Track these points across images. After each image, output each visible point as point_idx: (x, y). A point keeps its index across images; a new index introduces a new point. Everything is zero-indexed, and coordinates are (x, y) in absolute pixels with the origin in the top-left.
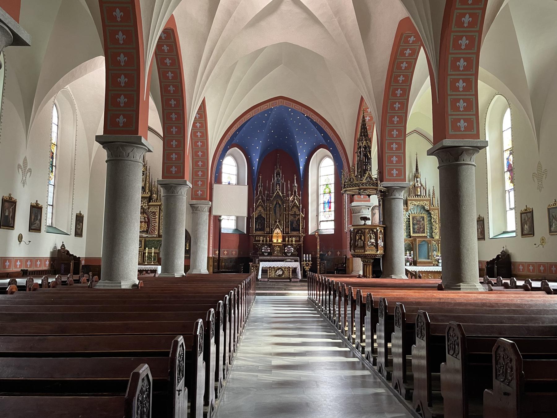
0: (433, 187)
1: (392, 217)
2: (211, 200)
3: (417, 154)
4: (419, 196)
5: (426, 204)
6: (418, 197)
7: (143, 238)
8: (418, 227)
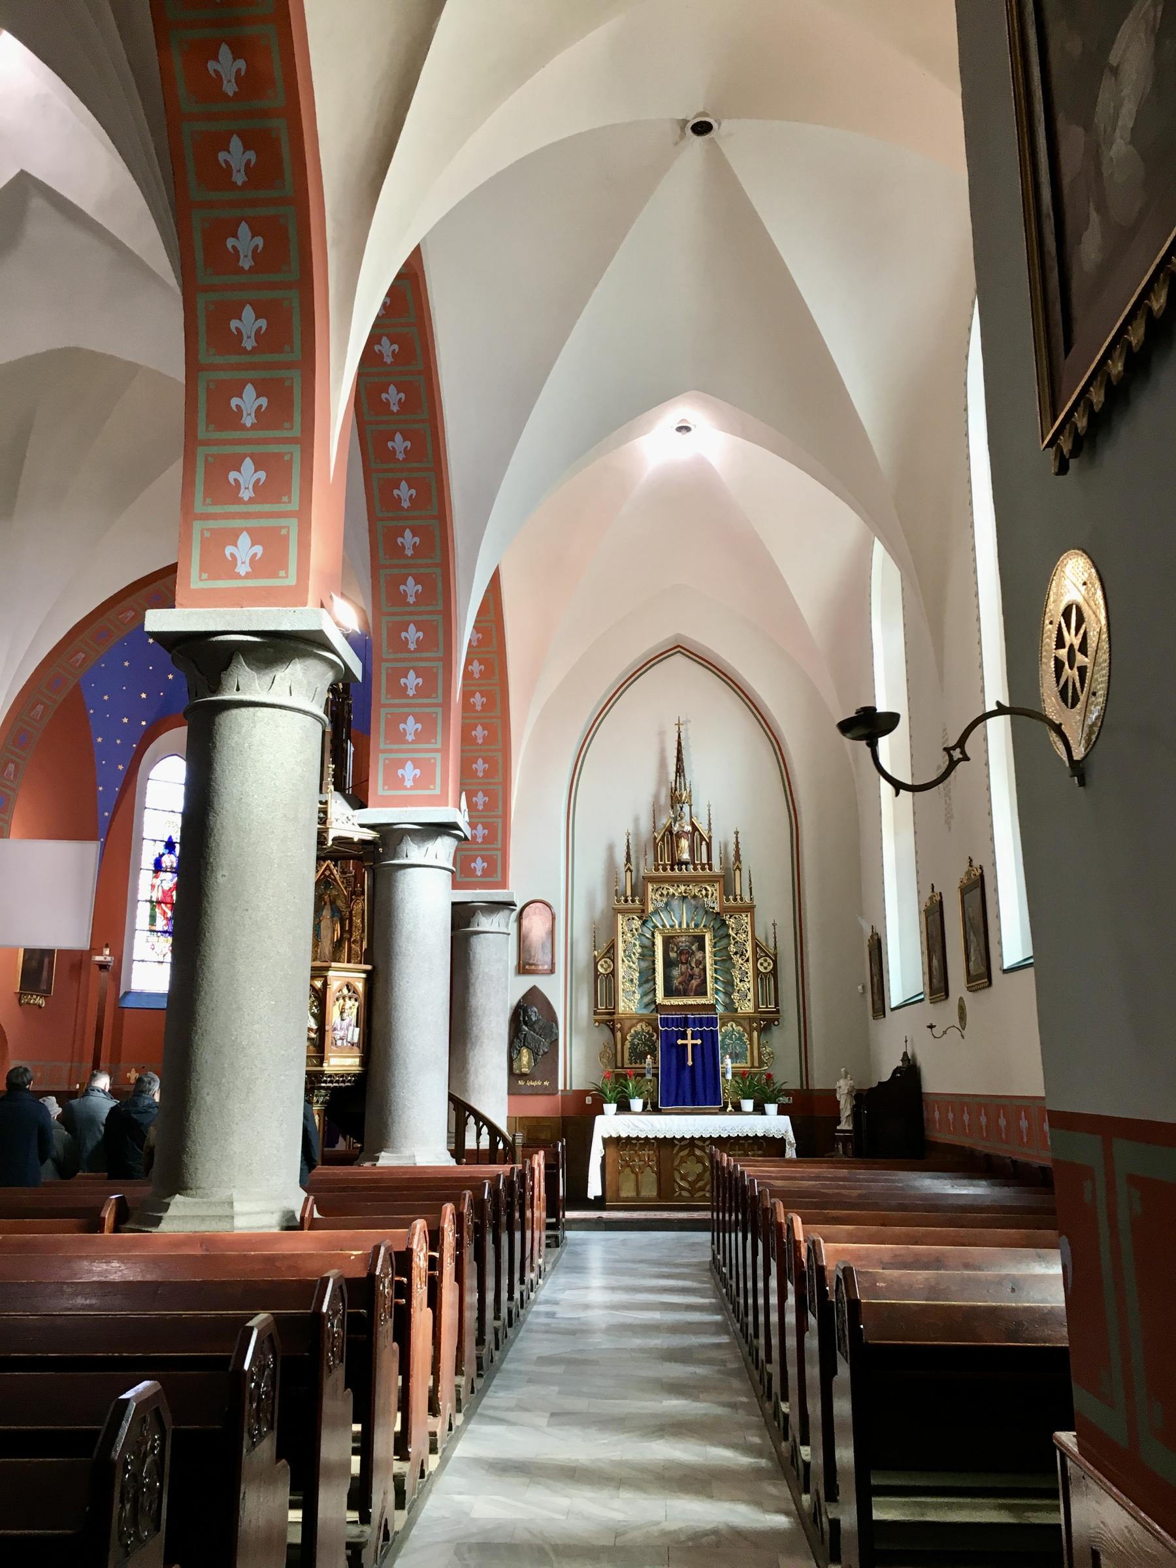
0: (737, 833)
3: (679, 724)
4: (684, 867)
5: (710, 893)
6: (680, 870)
8: (682, 974)
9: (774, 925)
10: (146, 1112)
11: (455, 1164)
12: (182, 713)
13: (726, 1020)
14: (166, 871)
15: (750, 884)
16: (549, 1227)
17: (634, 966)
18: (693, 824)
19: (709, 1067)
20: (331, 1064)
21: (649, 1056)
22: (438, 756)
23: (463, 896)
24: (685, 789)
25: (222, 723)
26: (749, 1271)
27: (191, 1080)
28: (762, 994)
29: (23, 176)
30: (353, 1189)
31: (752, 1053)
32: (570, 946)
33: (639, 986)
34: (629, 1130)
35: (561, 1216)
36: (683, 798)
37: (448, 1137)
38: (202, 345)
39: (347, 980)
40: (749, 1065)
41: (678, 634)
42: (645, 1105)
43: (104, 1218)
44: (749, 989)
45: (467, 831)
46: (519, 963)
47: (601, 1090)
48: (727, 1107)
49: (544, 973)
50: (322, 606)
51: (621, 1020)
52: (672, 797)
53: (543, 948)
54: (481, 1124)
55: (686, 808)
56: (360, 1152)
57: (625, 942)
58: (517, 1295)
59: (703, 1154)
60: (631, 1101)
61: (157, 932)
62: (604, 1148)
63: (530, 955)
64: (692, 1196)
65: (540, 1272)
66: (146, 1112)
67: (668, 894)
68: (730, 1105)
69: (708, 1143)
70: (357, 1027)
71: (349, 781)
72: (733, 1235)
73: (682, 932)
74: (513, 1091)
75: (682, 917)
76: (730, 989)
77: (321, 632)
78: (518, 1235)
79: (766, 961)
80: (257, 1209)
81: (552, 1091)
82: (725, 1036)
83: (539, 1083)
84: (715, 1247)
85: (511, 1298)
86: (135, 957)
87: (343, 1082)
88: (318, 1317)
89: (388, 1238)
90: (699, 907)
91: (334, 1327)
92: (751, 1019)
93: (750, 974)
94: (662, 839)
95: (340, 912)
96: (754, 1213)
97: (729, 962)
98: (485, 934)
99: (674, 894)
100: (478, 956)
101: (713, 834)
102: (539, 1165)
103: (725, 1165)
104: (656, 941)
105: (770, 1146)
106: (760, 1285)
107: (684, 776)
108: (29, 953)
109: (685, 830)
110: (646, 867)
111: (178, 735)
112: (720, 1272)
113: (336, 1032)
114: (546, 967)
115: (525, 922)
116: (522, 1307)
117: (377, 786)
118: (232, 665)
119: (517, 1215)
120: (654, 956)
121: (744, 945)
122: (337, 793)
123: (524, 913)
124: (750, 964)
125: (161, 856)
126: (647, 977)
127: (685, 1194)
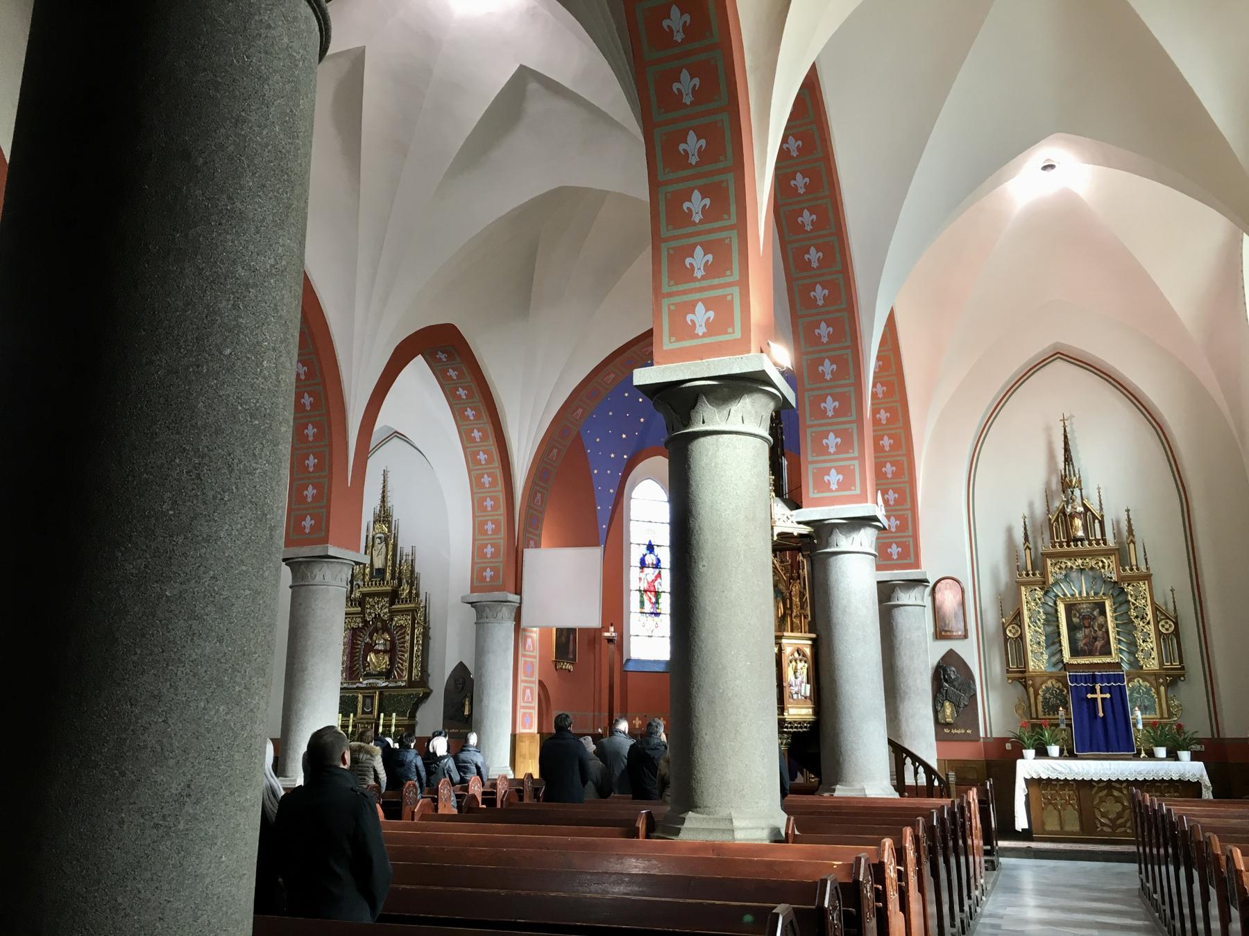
0: (1128, 511)
1: (829, 608)
2: (518, 591)
3: (1064, 420)
4: (1079, 543)
5: (1106, 564)
6: (1077, 546)
7: (374, 691)
8: (1086, 637)
9: (1172, 590)
10: (656, 749)
11: (899, 797)
12: (664, 447)
13: (1131, 677)
14: (649, 567)
15: (1145, 555)
16: (987, 853)
17: (1040, 630)
18: (1084, 506)
19: (1120, 718)
20: (790, 713)
21: (1061, 709)
22: (856, 463)
23: (886, 575)
24: (1075, 475)
25: (694, 449)
26: (1185, 900)
27: (692, 724)
28: (1166, 655)
29: (522, 69)
30: (821, 813)
31: (1160, 705)
32: (979, 614)
33: (1047, 648)
34: (1049, 773)
35: (995, 844)
36: (1074, 483)
37: (891, 775)
38: (660, 166)
39: (797, 646)
40: (1158, 716)
41: (1057, 343)
42: (1061, 752)
43: (639, 828)
44: (1152, 649)
45: (885, 522)
46: (936, 630)
47: (1020, 738)
48: (1140, 754)
49: (958, 638)
50: (762, 352)
51: (1032, 678)
52: (1062, 483)
53: (955, 617)
54: (917, 764)
55: (1077, 492)
56: (819, 785)
57: (1030, 610)
58: (966, 908)
59: (1120, 794)
60: (1048, 747)
61: (646, 613)
62: (1027, 788)
63: (945, 624)
64: (1114, 831)
65: (983, 890)
66: (656, 749)
67: (1066, 567)
68: (1143, 752)
69: (1125, 785)
70: (808, 683)
71: (786, 489)
72: (1163, 868)
73: (1082, 600)
74: (940, 738)
75: (1081, 587)
76: (1133, 649)
77: (764, 371)
78: (963, 859)
79: (1167, 623)
80: (750, 825)
81: (977, 739)
82: (1132, 690)
83: (963, 731)
84: (1143, 876)
85: (962, 910)
86: (632, 633)
87: (801, 728)
88: (822, 911)
89: (865, 853)
90: (1096, 577)
91: (834, 919)
92: (1156, 675)
93: (1153, 635)
94: (1057, 520)
95: (782, 593)
96: (1186, 847)
97: (1131, 625)
98: (904, 607)
99: (1072, 568)
100: (900, 626)
101: (1105, 512)
102: (973, 799)
103: (1149, 804)
104: (1059, 608)
105: (1188, 789)
106: (1199, 912)
107: (1072, 464)
108: (560, 631)
109: (1078, 510)
110: (1044, 545)
111: (660, 463)
112: (1150, 898)
113: (792, 688)
114: (960, 633)
115: (938, 596)
116: (971, 919)
117: (809, 491)
118: (699, 403)
119: (961, 842)
120: (1058, 621)
121: (1144, 609)
122: (777, 498)
123: (937, 589)
124: (1152, 626)
125: (644, 556)
126: (1053, 640)
127: (1106, 829)
